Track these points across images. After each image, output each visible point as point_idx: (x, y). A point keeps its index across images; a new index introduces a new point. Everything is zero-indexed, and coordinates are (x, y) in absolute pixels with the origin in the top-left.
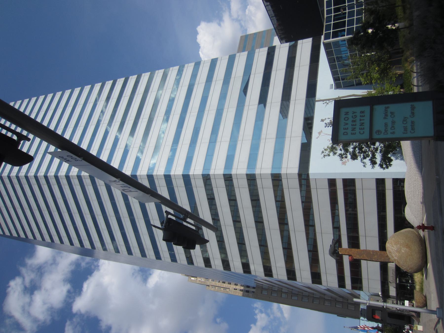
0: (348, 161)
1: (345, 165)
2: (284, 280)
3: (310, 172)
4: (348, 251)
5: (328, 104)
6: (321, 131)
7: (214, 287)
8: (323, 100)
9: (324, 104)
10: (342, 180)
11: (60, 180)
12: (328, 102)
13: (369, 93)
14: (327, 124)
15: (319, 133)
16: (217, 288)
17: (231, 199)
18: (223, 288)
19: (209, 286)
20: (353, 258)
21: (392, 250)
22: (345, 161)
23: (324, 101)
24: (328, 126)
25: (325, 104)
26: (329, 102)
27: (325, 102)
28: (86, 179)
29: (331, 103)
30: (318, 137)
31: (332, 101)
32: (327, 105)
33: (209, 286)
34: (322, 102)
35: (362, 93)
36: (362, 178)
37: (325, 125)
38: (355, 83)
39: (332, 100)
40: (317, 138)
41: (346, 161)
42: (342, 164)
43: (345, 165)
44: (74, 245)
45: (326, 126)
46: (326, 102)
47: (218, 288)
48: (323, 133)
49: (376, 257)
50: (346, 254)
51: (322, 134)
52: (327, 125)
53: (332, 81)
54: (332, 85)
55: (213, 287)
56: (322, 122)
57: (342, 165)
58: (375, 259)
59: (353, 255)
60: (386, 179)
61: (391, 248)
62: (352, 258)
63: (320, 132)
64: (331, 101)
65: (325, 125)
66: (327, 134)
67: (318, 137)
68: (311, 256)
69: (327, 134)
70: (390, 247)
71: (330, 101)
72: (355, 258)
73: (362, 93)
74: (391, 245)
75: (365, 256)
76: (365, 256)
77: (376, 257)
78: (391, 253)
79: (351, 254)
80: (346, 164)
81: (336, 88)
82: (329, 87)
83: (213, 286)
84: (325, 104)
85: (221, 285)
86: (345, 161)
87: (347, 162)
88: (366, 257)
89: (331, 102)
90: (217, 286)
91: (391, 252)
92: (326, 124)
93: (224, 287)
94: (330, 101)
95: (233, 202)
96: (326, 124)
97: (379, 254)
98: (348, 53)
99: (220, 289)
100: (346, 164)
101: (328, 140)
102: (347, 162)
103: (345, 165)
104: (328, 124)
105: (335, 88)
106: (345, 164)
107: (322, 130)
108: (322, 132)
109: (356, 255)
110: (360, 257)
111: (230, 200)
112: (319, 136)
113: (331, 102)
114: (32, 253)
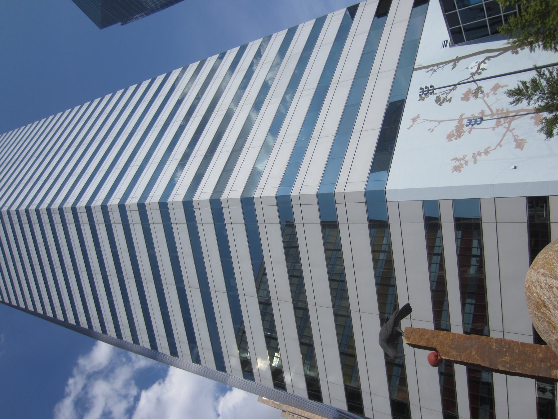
0: (466, 165)
1: (460, 171)
2: (344, 410)
3: (388, 188)
4: (427, 336)
5: (435, 71)
6: (418, 117)
7: (293, 414)
8: (427, 67)
9: (428, 72)
10: (450, 203)
11: (33, 224)
12: (435, 68)
13: (519, 35)
14: (425, 90)
15: (414, 120)
16: (295, 416)
17: (294, 275)
18: (304, 417)
19: (285, 412)
20: (439, 358)
21: (548, 294)
22: (461, 164)
23: (428, 69)
24: (426, 92)
25: (431, 71)
26: (438, 68)
27: (430, 69)
28: (44, 215)
29: (442, 69)
30: (411, 126)
31: (444, 66)
32: (433, 73)
33: (285, 412)
34: (425, 70)
35: (504, 44)
36: (495, 198)
37: (420, 92)
38: (490, 31)
39: (444, 65)
40: (409, 128)
41: (463, 163)
42: (452, 171)
43: (459, 173)
44: (140, 344)
45: (421, 93)
46: (433, 68)
47: (297, 417)
48: (420, 118)
49: (507, 358)
50: (421, 344)
51: (418, 121)
52: (423, 91)
53: (446, 36)
54: (447, 41)
55: (290, 414)
56: (421, 101)
57: (453, 172)
58: (504, 366)
59: (438, 348)
60: (551, 199)
61: (546, 284)
62: (436, 356)
63: (415, 118)
64: (441, 66)
65: (420, 92)
66: (427, 120)
67: (411, 126)
68: (442, 384)
69: (427, 120)
70: (542, 278)
71: (439, 67)
72: (444, 357)
73: (504, 44)
74: (547, 272)
75: (474, 353)
76: (474, 353)
77: (507, 358)
78: (545, 306)
79: (434, 346)
80: (461, 169)
81: (452, 45)
82: (441, 44)
83: (291, 413)
84: (431, 72)
85: (301, 413)
86: (461, 164)
87: (464, 165)
88: (476, 356)
89: (442, 68)
90: (296, 413)
91: (547, 304)
92: (422, 91)
93: (299, 414)
94: (439, 67)
95: (295, 280)
96: (422, 91)
97: (517, 351)
98: (482, 2)
99: (300, 418)
100: (461, 169)
101: (430, 129)
102: (464, 165)
103: (459, 173)
104: (427, 89)
105: (451, 45)
106: (458, 169)
107: (419, 115)
108: (420, 117)
109: (448, 349)
110: (461, 358)
111: (291, 276)
112: (413, 124)
113: (441, 67)
114: (87, 350)
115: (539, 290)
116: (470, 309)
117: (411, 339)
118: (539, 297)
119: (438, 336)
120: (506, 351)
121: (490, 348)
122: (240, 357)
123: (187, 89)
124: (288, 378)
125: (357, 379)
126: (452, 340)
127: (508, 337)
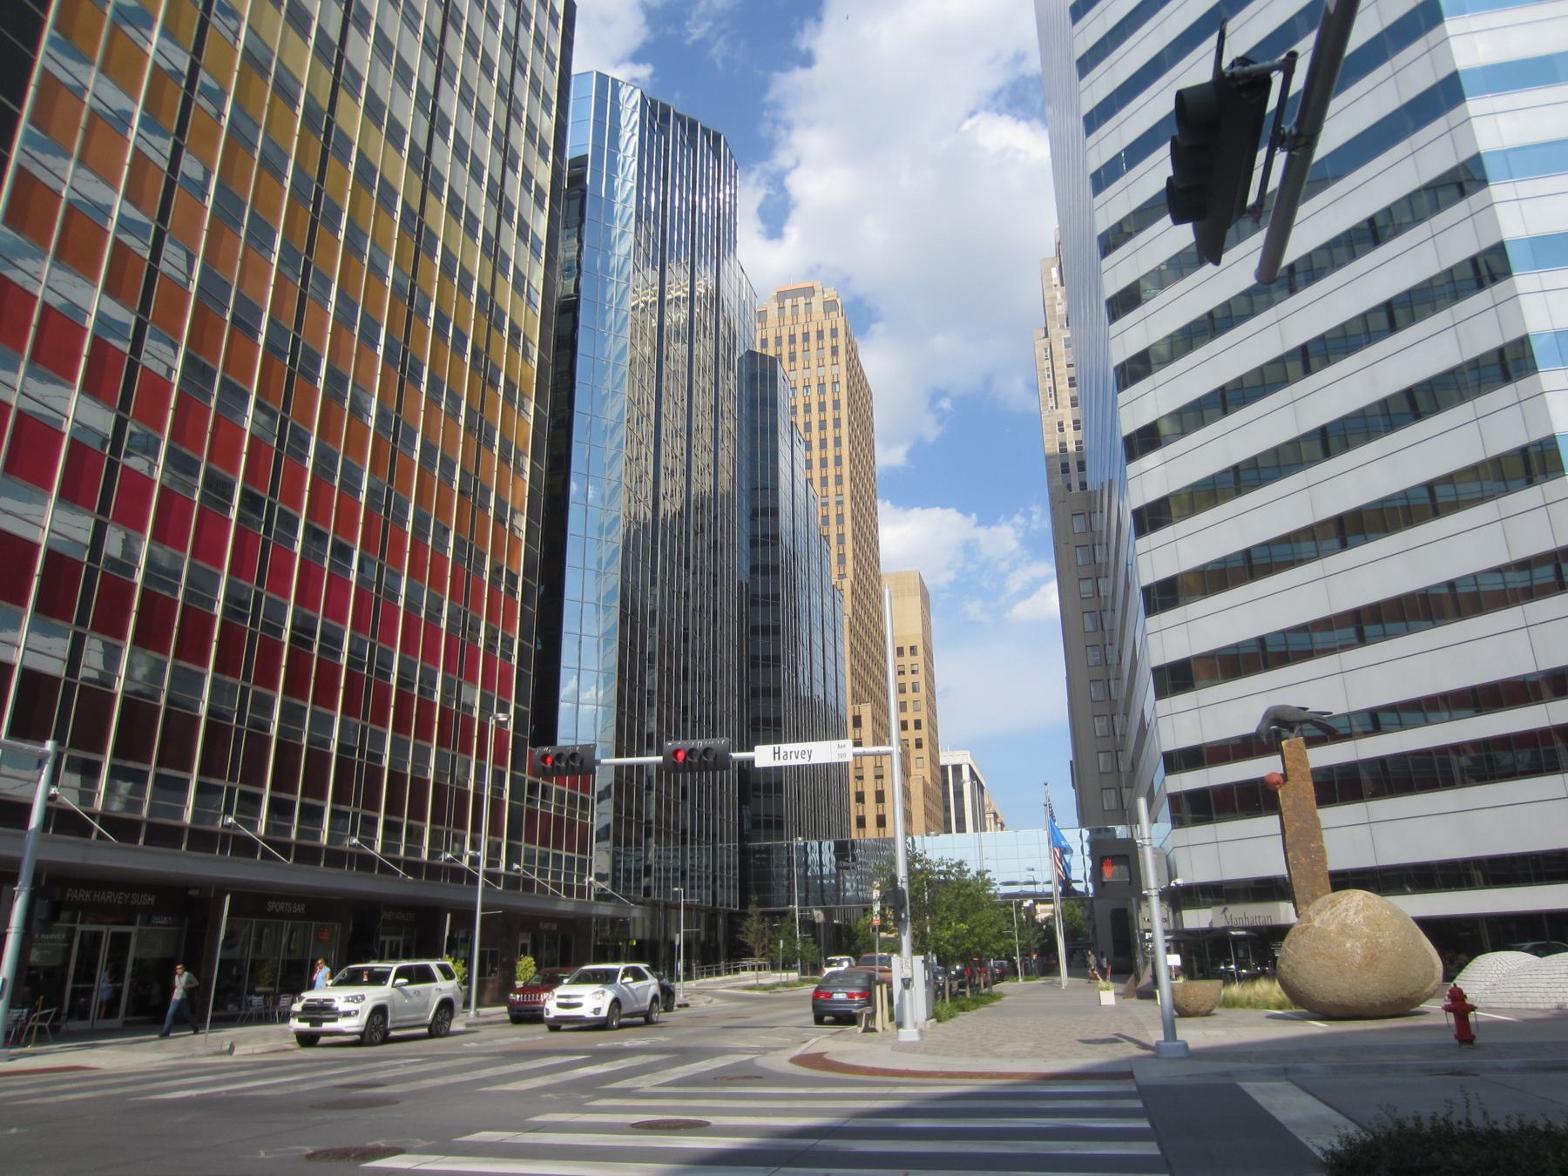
4: (1299, 767)
33: (1046, 336)
49: (1303, 860)
58: (1293, 858)
59: (1289, 784)
70: (1354, 904)
75: (1297, 824)
99: (1049, 376)
115: (1345, 902)
116: (1494, 583)
117: (1291, 749)
118: (1340, 903)
119: (1304, 780)
120: (1311, 858)
121: (1310, 842)
122: (1137, 282)
123: (1392, 717)
124: (1151, 460)
125: (1184, 516)
126: (1305, 798)
127: (1510, 586)
